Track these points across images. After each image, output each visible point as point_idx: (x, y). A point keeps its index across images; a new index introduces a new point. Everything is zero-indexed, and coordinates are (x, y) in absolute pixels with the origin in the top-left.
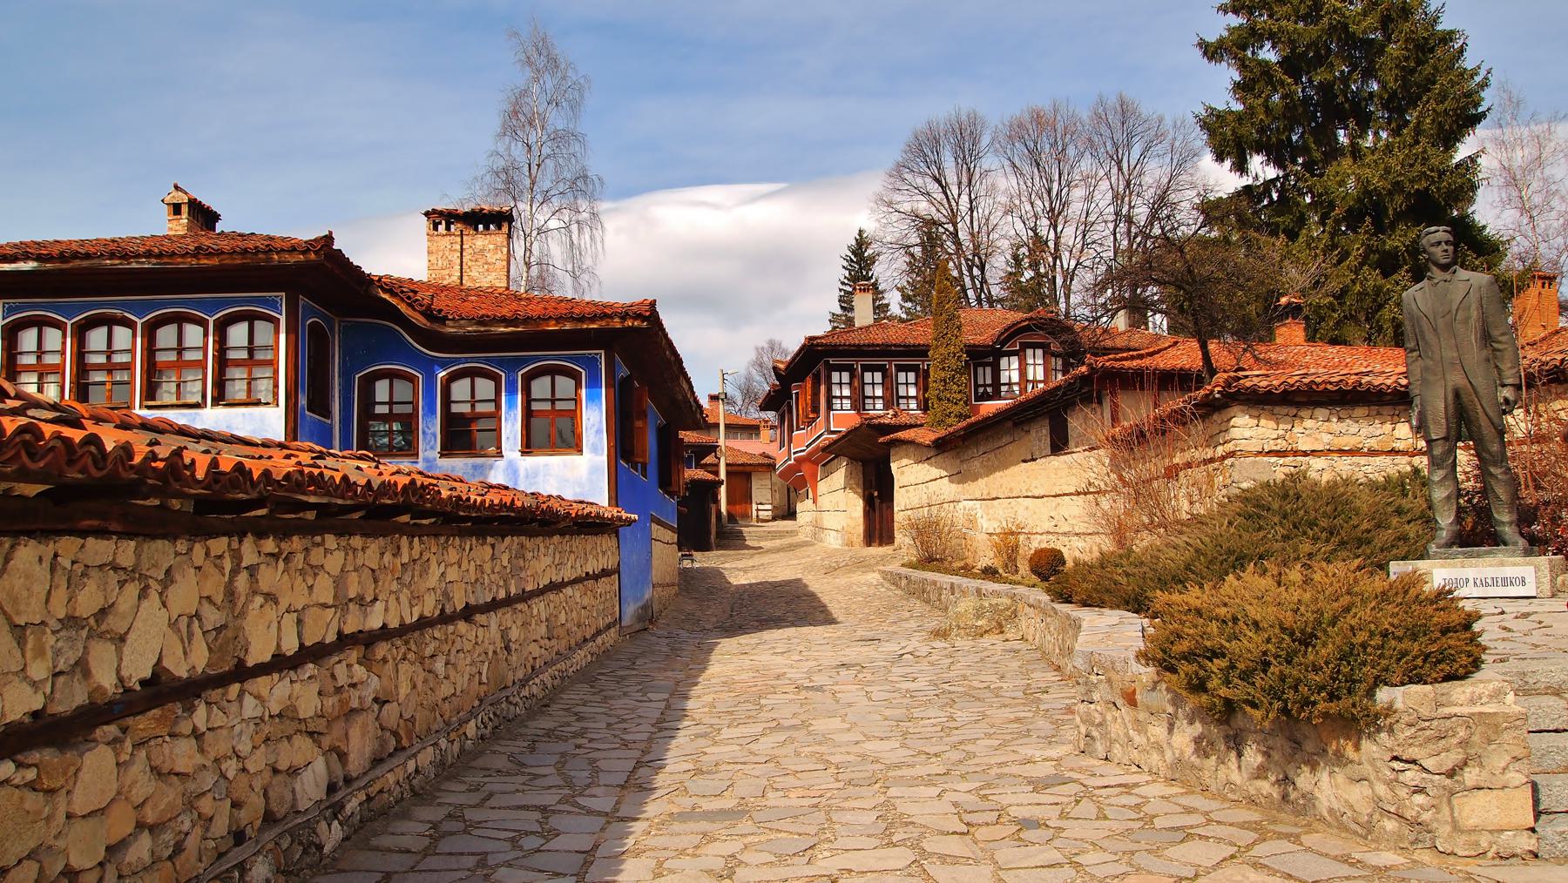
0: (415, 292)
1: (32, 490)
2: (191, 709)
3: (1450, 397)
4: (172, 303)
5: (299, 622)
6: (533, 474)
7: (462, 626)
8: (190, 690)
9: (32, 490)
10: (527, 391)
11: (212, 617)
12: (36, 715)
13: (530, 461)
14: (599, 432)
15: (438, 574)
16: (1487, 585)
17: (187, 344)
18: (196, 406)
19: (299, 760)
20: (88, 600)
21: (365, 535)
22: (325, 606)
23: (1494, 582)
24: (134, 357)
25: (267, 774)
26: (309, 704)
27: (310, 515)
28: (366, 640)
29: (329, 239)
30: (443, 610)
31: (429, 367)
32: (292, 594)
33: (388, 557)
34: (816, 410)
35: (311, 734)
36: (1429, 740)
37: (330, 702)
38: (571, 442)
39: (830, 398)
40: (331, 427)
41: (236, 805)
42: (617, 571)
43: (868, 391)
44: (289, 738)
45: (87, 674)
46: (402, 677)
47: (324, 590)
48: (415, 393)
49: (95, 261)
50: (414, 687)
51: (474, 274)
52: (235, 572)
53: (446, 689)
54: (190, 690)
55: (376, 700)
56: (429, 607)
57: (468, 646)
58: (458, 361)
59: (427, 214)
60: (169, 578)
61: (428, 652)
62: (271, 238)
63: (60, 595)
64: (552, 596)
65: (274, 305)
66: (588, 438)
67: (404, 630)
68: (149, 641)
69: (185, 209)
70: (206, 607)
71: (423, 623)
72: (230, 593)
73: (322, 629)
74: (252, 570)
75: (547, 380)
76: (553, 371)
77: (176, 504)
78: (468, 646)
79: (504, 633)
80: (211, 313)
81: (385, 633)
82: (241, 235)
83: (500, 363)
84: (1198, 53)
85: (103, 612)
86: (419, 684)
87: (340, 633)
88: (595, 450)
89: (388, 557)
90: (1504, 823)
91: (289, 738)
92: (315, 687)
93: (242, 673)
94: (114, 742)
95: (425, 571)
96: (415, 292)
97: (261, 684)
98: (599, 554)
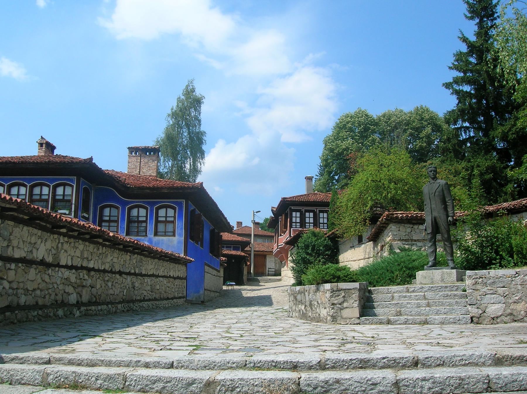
0: (120, 178)
1: (26, 217)
2: (48, 270)
4: (39, 179)
5: (72, 259)
6: (158, 243)
7: (118, 276)
8: (48, 265)
9: (26, 217)
10: (157, 213)
11: (54, 252)
12: (25, 257)
13: (157, 238)
15: (111, 258)
17: (43, 193)
19: (70, 292)
20: (33, 240)
21: (90, 243)
22: (78, 257)
24: (26, 197)
25: (63, 292)
26: (73, 279)
27: (76, 234)
28: (89, 270)
29: (91, 159)
30: (111, 269)
31: (124, 204)
32: (72, 252)
33: (95, 250)
34: (286, 227)
35: (73, 287)
36: (336, 296)
37: (78, 281)
39: (291, 222)
41: (56, 295)
42: (186, 279)
43: (307, 220)
44: (68, 285)
45: (32, 253)
46: (98, 283)
47: (78, 253)
48: (118, 213)
50: (101, 287)
52: (59, 243)
53: (111, 292)
54: (48, 265)
55: (90, 286)
56: (107, 267)
57: (119, 282)
59: (129, 148)
60: (46, 240)
61: (106, 279)
62: (73, 158)
63: (29, 237)
64: (153, 278)
65: (72, 181)
67: (98, 271)
68: (41, 252)
69: (44, 145)
70: (52, 249)
71: (104, 271)
72: (57, 247)
73: (77, 262)
74: (62, 243)
75: (164, 210)
76: (166, 207)
77: (48, 225)
78: (119, 282)
79: (133, 283)
80: (51, 183)
81: (93, 269)
82: (62, 156)
83: (148, 203)
85: (35, 243)
86: (103, 287)
87: (82, 265)
88: (180, 235)
89: (95, 250)
90: (352, 316)
91: (68, 285)
92: (75, 276)
93: (59, 266)
94: (35, 269)
95: (106, 256)
96: (120, 178)
97: (63, 270)
98: (179, 271)
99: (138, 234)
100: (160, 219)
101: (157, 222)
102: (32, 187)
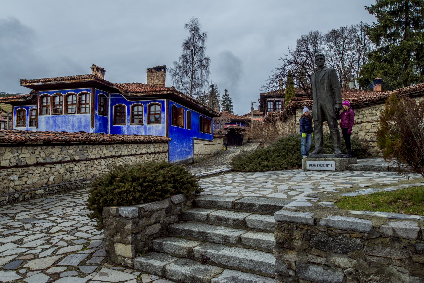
3: (319, 107)
14: (164, 119)
16: (321, 166)
17: (157, 110)
18: (74, 113)
23: (323, 165)
32: (105, 151)
38: (157, 121)
40: (107, 119)
49: (52, 82)
51: (157, 82)
58: (134, 102)
65: (89, 91)
66: (162, 120)
69: (95, 69)
75: (154, 106)
84: (368, 12)
88: (163, 123)
99: (101, 117)
100: (152, 113)
101: (149, 114)
102: (67, 97)
